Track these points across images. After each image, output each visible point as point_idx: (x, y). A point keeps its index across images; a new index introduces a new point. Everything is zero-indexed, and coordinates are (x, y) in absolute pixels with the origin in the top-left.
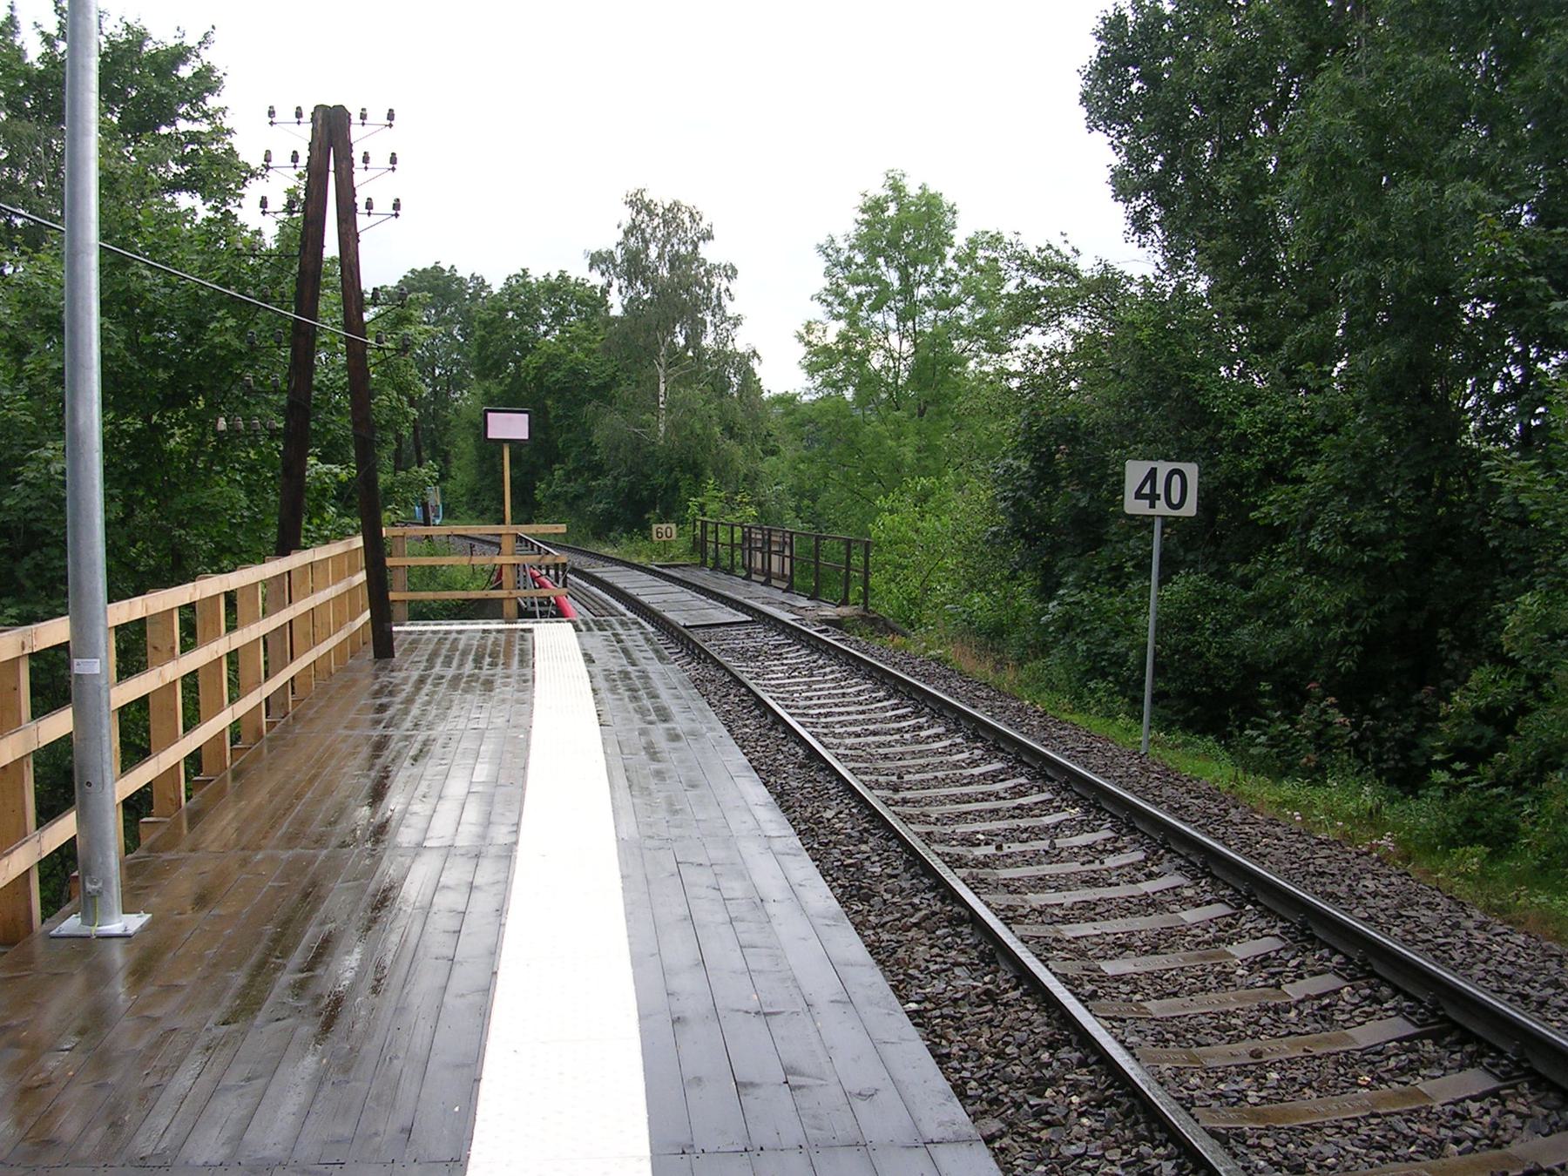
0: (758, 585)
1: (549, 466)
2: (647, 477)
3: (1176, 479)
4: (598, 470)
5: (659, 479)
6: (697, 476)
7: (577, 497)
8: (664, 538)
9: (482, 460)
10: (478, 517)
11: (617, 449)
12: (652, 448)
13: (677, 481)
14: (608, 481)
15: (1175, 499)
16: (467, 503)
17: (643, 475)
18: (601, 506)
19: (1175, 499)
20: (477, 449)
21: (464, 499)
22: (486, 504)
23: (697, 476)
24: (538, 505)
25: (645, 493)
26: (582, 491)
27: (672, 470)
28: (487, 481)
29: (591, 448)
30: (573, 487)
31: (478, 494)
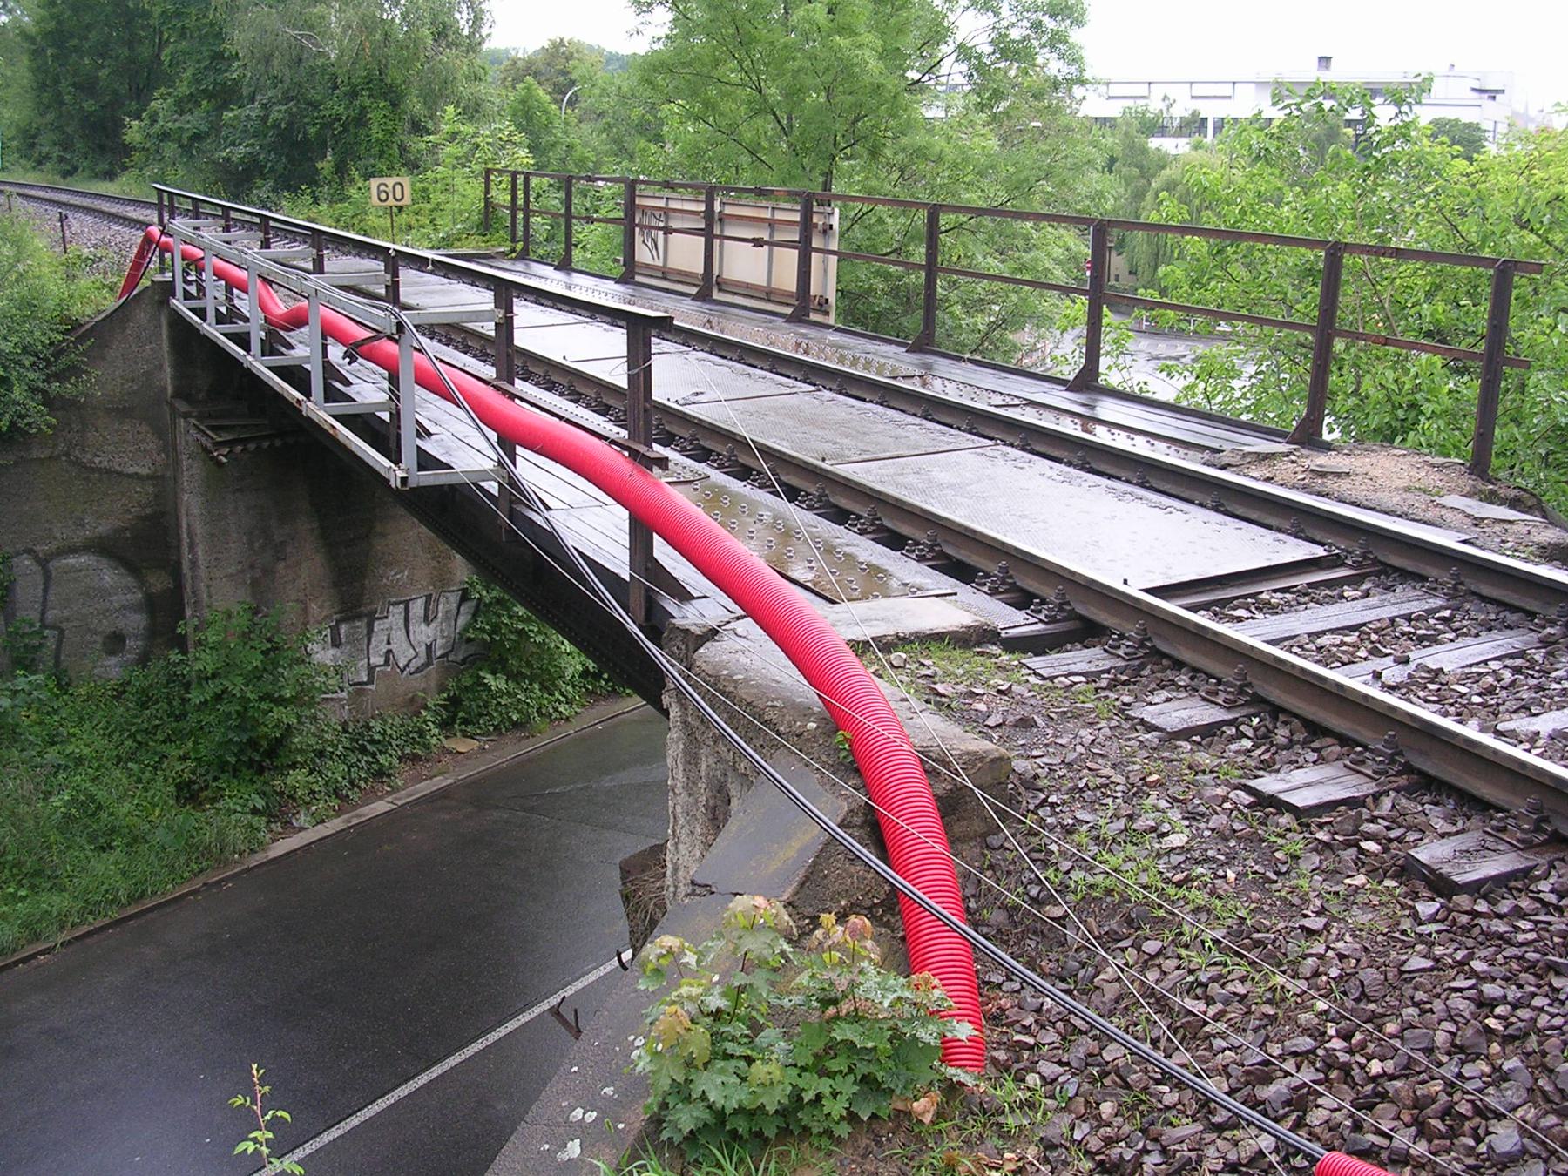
0: (689, 301)
1: (141, 94)
2: (314, 105)
3: (398, 187)
4: (226, 96)
5: (336, 107)
6: (394, 105)
7: (197, 137)
8: (391, 202)
9: (43, 87)
10: (34, 168)
11: (267, 60)
12: (319, 62)
13: (363, 110)
14: (253, 111)
15: (399, 196)
16: (18, 150)
17: (309, 104)
18: (241, 149)
19: (399, 196)
20: (33, 71)
21: (15, 143)
22: (45, 150)
23: (394, 105)
24: (127, 150)
25: (312, 130)
26: (204, 128)
27: (353, 94)
28: (50, 117)
29: (220, 59)
30: (194, 121)
31: (34, 137)
